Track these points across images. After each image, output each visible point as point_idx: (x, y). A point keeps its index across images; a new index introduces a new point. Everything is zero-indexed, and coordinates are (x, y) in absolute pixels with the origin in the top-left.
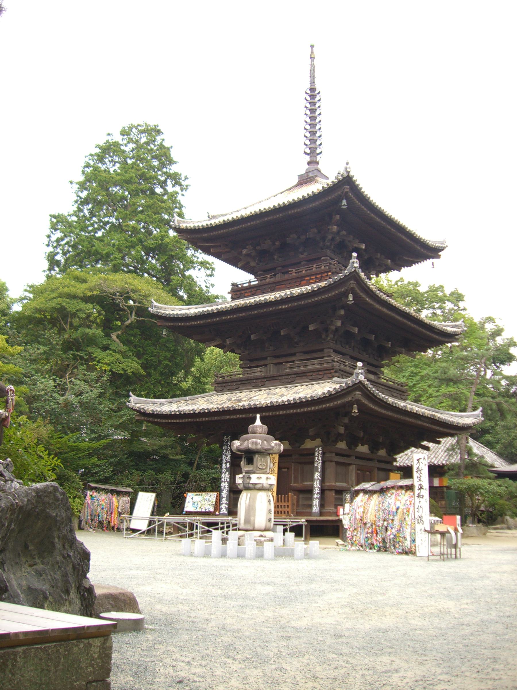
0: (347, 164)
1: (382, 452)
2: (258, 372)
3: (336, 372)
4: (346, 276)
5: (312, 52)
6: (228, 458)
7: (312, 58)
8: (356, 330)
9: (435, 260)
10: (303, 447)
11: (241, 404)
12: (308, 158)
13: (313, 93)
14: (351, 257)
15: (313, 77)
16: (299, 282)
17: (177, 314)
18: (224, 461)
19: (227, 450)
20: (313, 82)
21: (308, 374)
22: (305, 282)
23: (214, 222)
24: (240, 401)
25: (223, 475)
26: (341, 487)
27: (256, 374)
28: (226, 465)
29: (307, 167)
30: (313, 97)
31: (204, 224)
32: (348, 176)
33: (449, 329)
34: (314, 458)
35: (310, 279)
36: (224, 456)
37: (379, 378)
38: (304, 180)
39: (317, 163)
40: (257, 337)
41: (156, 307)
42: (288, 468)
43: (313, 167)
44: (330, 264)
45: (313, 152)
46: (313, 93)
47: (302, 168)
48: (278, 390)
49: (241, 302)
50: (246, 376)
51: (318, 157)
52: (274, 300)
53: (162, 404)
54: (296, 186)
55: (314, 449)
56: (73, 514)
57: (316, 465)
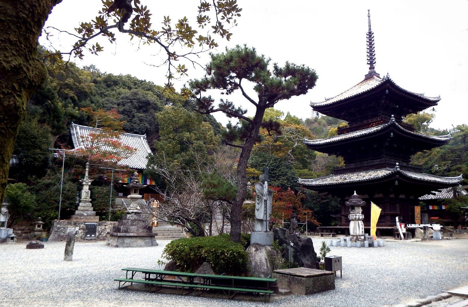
2: (352, 166)
3: (387, 165)
4: (389, 125)
5: (369, 13)
7: (369, 17)
9: (435, 107)
10: (375, 197)
11: (346, 181)
12: (369, 66)
13: (370, 34)
14: (391, 117)
15: (370, 26)
16: (367, 126)
20: (370, 29)
24: (346, 179)
26: (416, 175)
27: (351, 167)
29: (369, 70)
30: (370, 36)
32: (388, 80)
33: (443, 139)
37: (408, 164)
38: (369, 77)
39: (374, 68)
40: (352, 154)
41: (306, 141)
43: (372, 70)
44: (382, 117)
45: (371, 62)
46: (370, 34)
47: (366, 70)
48: (361, 174)
50: (348, 167)
53: (312, 181)
54: (364, 80)
56: (19, 55)
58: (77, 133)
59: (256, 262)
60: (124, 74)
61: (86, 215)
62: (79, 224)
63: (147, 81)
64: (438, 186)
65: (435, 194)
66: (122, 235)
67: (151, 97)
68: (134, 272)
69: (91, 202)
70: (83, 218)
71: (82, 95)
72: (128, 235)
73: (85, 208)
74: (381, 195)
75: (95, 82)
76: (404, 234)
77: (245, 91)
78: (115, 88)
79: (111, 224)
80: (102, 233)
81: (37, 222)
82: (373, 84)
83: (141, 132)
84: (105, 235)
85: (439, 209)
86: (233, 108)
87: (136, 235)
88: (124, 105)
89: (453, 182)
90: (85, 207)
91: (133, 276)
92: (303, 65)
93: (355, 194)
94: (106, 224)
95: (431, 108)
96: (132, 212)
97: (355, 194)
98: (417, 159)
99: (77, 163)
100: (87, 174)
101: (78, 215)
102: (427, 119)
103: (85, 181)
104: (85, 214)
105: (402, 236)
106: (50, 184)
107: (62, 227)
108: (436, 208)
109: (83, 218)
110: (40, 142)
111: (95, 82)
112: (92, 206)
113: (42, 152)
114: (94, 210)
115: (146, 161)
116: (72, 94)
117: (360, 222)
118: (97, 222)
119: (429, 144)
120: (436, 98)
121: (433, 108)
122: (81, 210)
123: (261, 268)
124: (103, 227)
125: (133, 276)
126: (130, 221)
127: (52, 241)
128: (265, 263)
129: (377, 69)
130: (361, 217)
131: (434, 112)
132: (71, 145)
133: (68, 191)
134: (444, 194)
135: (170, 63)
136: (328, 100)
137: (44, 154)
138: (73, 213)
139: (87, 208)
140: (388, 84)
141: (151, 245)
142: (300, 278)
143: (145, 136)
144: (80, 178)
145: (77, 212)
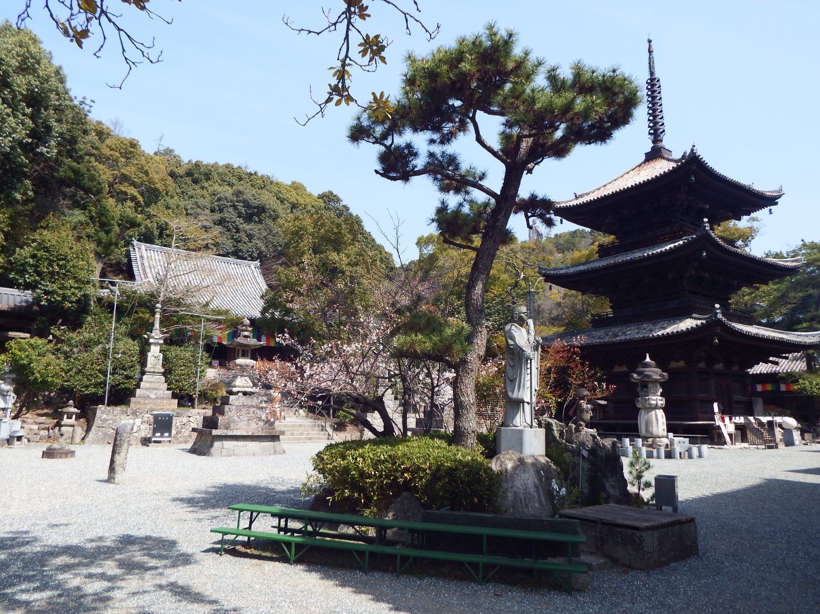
1: (735, 368)
5: (650, 46)
7: (650, 52)
8: (707, 275)
9: (772, 207)
11: (618, 338)
20: (652, 73)
23: (580, 201)
24: (616, 336)
38: (655, 154)
47: (648, 146)
48: (645, 326)
49: (611, 261)
51: (662, 135)
58: (142, 257)
59: (515, 492)
60: (222, 162)
61: (155, 397)
62: (141, 413)
63: (260, 174)
64: (782, 349)
65: (777, 363)
66: (219, 434)
67: (267, 199)
68: (255, 514)
69: (164, 374)
70: (148, 403)
71: (152, 195)
72: (230, 433)
73: (152, 386)
74: (681, 364)
75: (172, 175)
76: (730, 435)
77: (481, 133)
78: (206, 184)
79: (198, 413)
80: (183, 430)
81: (65, 410)
82: (660, 167)
83: (250, 256)
84: (187, 433)
85: (775, 389)
86: (457, 167)
87: (245, 434)
88: (221, 211)
89: (811, 341)
90: (153, 390)
91: (251, 522)
92: (614, 71)
93: (648, 359)
94: (189, 414)
95: (766, 210)
96: (238, 392)
97: (648, 359)
98: (744, 296)
99: (140, 305)
100: (157, 325)
101: (140, 397)
102: (747, 236)
103: (153, 338)
104: (153, 396)
105: (728, 438)
106: (90, 340)
107: (111, 419)
108: (769, 387)
109: (148, 403)
110: (74, 266)
111: (172, 175)
112: (166, 382)
113: (76, 285)
114: (168, 389)
115: (261, 304)
116: (132, 191)
117: (658, 411)
118: (173, 410)
119: (763, 271)
120: (775, 191)
121: (770, 210)
122: (147, 389)
123: (527, 506)
124: (185, 420)
125: (251, 522)
126: (234, 407)
127: (93, 443)
128: (535, 494)
129: (667, 142)
130: (660, 403)
131: (755, 224)
132: (131, 276)
133: (124, 353)
134: (788, 365)
135: (349, 23)
136: (581, 196)
137: (80, 288)
138: (132, 393)
139: (156, 385)
140: (692, 164)
141: (272, 452)
142: (630, 531)
143: (258, 263)
144: (143, 332)
145: (138, 391)
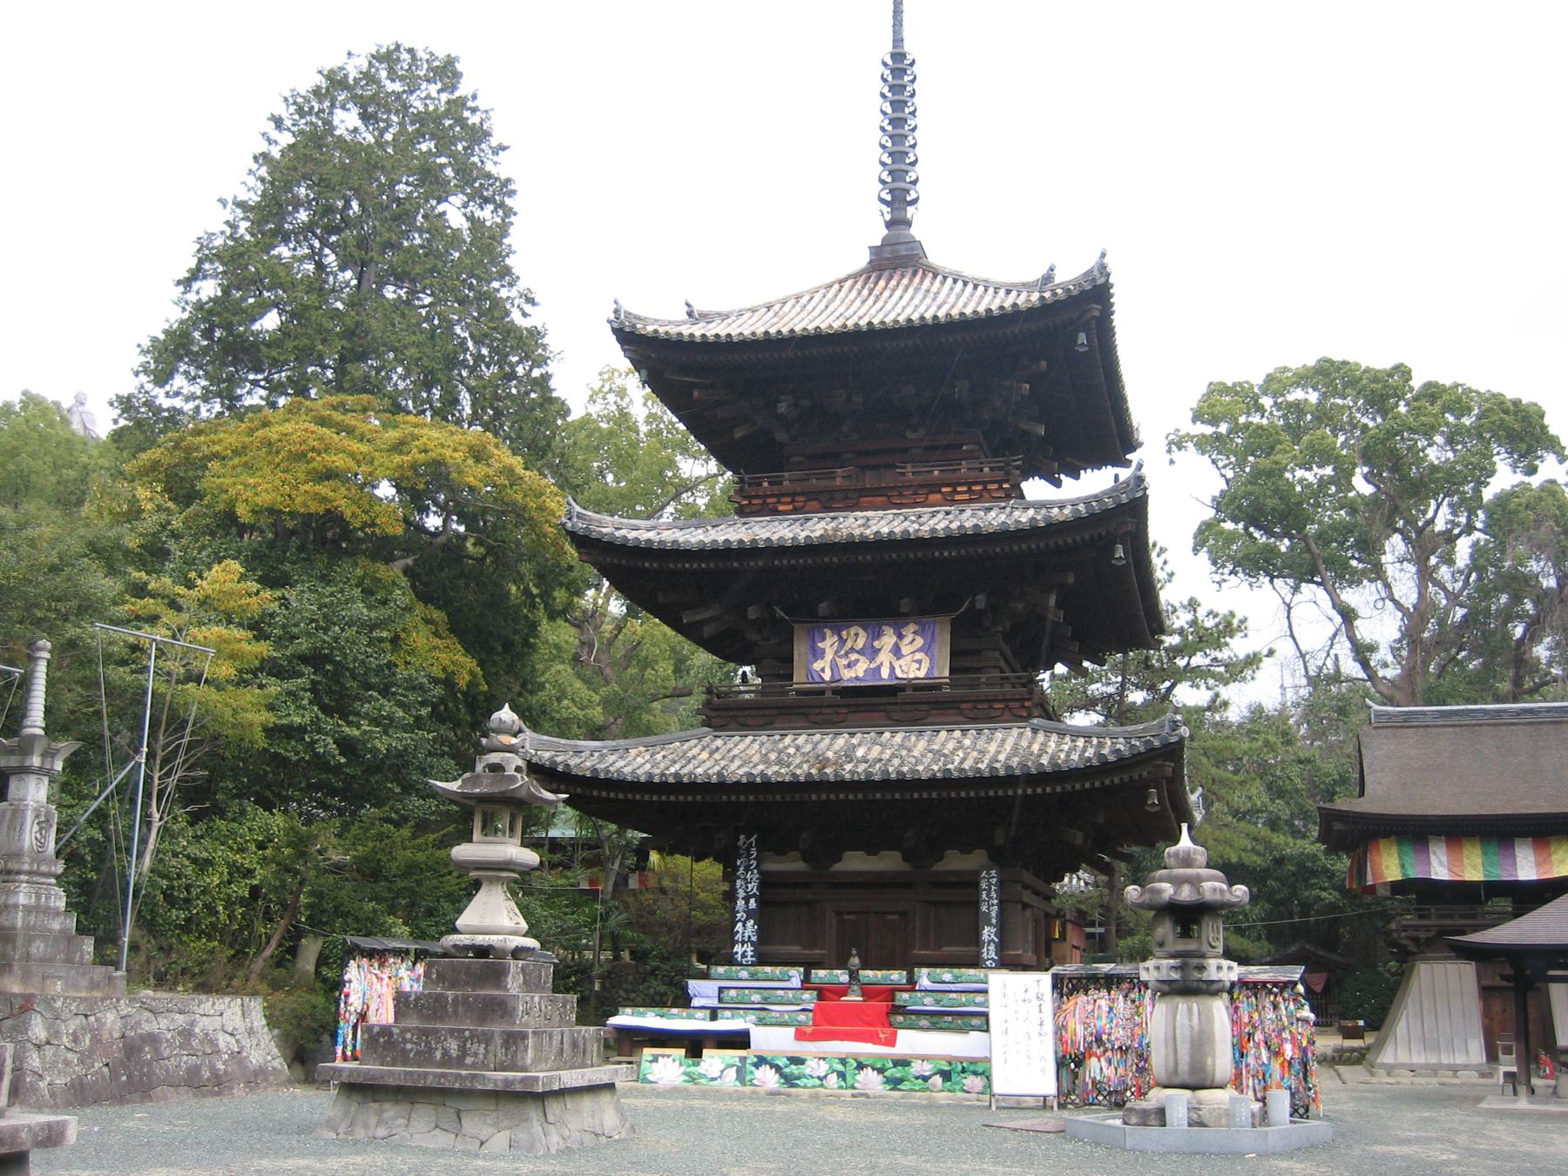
0: (1103, 255)
6: (753, 887)
10: (939, 867)
13: (899, 67)
17: (675, 542)
18: (741, 893)
19: (747, 869)
20: (898, 40)
21: (963, 706)
22: (938, 496)
23: (698, 331)
25: (739, 927)
28: (747, 903)
30: (899, 72)
31: (673, 330)
34: (978, 894)
35: (955, 492)
36: (739, 882)
42: (904, 914)
46: (899, 67)
52: (927, 536)
55: (977, 874)
57: (984, 908)
